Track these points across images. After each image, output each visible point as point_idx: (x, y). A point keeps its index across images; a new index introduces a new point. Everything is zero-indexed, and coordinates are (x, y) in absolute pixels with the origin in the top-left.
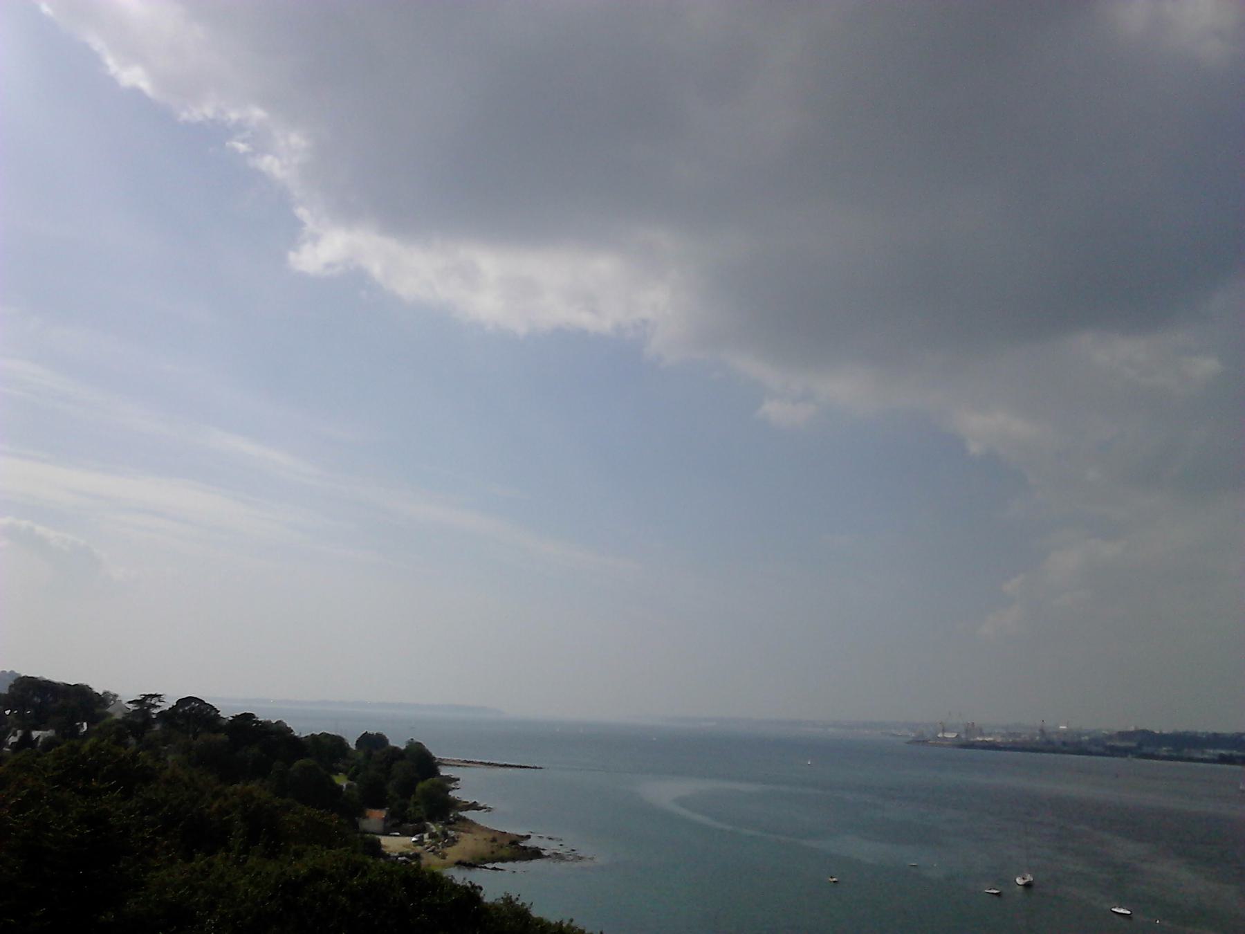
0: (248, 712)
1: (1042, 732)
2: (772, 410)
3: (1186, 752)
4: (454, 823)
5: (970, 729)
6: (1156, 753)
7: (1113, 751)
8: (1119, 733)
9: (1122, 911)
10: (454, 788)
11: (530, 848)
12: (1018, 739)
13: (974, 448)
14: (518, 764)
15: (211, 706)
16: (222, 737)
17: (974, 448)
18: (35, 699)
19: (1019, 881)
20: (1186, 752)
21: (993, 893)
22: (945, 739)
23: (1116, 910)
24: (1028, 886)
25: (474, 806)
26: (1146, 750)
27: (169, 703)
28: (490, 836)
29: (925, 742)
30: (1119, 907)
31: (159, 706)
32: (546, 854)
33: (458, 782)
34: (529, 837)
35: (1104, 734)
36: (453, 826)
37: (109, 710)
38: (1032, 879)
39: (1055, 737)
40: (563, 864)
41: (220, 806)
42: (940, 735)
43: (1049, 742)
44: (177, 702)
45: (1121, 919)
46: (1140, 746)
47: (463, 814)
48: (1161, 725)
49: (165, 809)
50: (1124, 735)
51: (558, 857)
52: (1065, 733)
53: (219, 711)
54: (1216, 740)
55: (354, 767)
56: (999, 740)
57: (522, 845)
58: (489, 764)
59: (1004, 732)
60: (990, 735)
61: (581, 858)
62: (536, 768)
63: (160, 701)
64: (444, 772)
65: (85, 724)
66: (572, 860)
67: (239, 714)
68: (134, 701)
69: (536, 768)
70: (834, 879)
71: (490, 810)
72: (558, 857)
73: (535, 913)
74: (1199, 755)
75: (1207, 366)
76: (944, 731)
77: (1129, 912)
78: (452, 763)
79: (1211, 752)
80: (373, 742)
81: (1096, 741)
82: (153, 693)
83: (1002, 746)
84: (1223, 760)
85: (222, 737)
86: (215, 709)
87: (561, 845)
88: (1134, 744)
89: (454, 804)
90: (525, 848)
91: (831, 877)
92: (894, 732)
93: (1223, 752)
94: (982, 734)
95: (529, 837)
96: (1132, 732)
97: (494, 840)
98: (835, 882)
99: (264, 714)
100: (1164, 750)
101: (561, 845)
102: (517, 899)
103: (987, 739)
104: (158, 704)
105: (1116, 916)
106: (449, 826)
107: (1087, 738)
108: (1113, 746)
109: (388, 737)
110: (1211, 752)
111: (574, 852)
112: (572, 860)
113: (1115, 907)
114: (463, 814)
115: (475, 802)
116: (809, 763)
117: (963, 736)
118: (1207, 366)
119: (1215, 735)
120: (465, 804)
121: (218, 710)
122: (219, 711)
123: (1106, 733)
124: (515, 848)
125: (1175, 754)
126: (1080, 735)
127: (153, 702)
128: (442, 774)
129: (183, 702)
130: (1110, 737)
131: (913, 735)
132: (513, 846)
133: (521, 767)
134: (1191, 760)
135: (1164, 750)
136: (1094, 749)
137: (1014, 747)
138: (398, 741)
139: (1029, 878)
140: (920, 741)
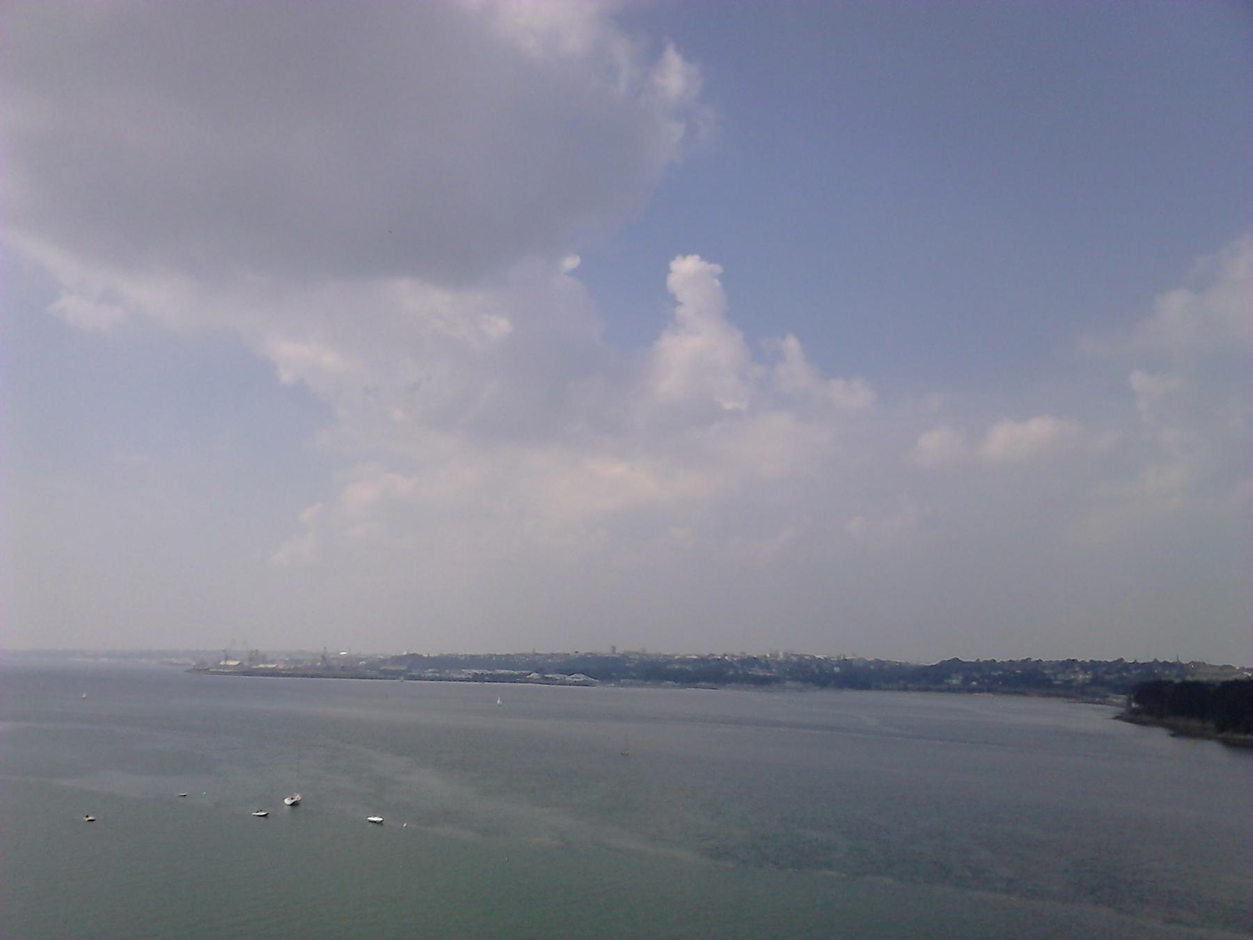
1: (324, 658)
5: (255, 656)
6: (422, 676)
7: (387, 675)
8: (393, 657)
12: (300, 666)
13: (286, 377)
17: (286, 377)
18: (835, 669)
19: (288, 801)
21: (375, 822)
22: (226, 667)
35: (380, 659)
42: (222, 663)
46: (409, 669)
48: (820, 651)
50: (398, 660)
52: (346, 658)
54: (473, 661)
56: (281, 667)
60: (273, 662)
70: (90, 818)
75: (500, 326)
76: (227, 659)
77: (381, 819)
84: (476, 678)
88: (404, 668)
94: (265, 662)
96: (405, 656)
100: (429, 672)
103: (270, 666)
105: (371, 825)
116: (84, 696)
117: (246, 664)
118: (500, 326)
119: (472, 656)
123: (382, 657)
126: (669, 662)
130: (384, 662)
135: (429, 672)
136: (369, 673)
139: (297, 797)
140: (201, 669)
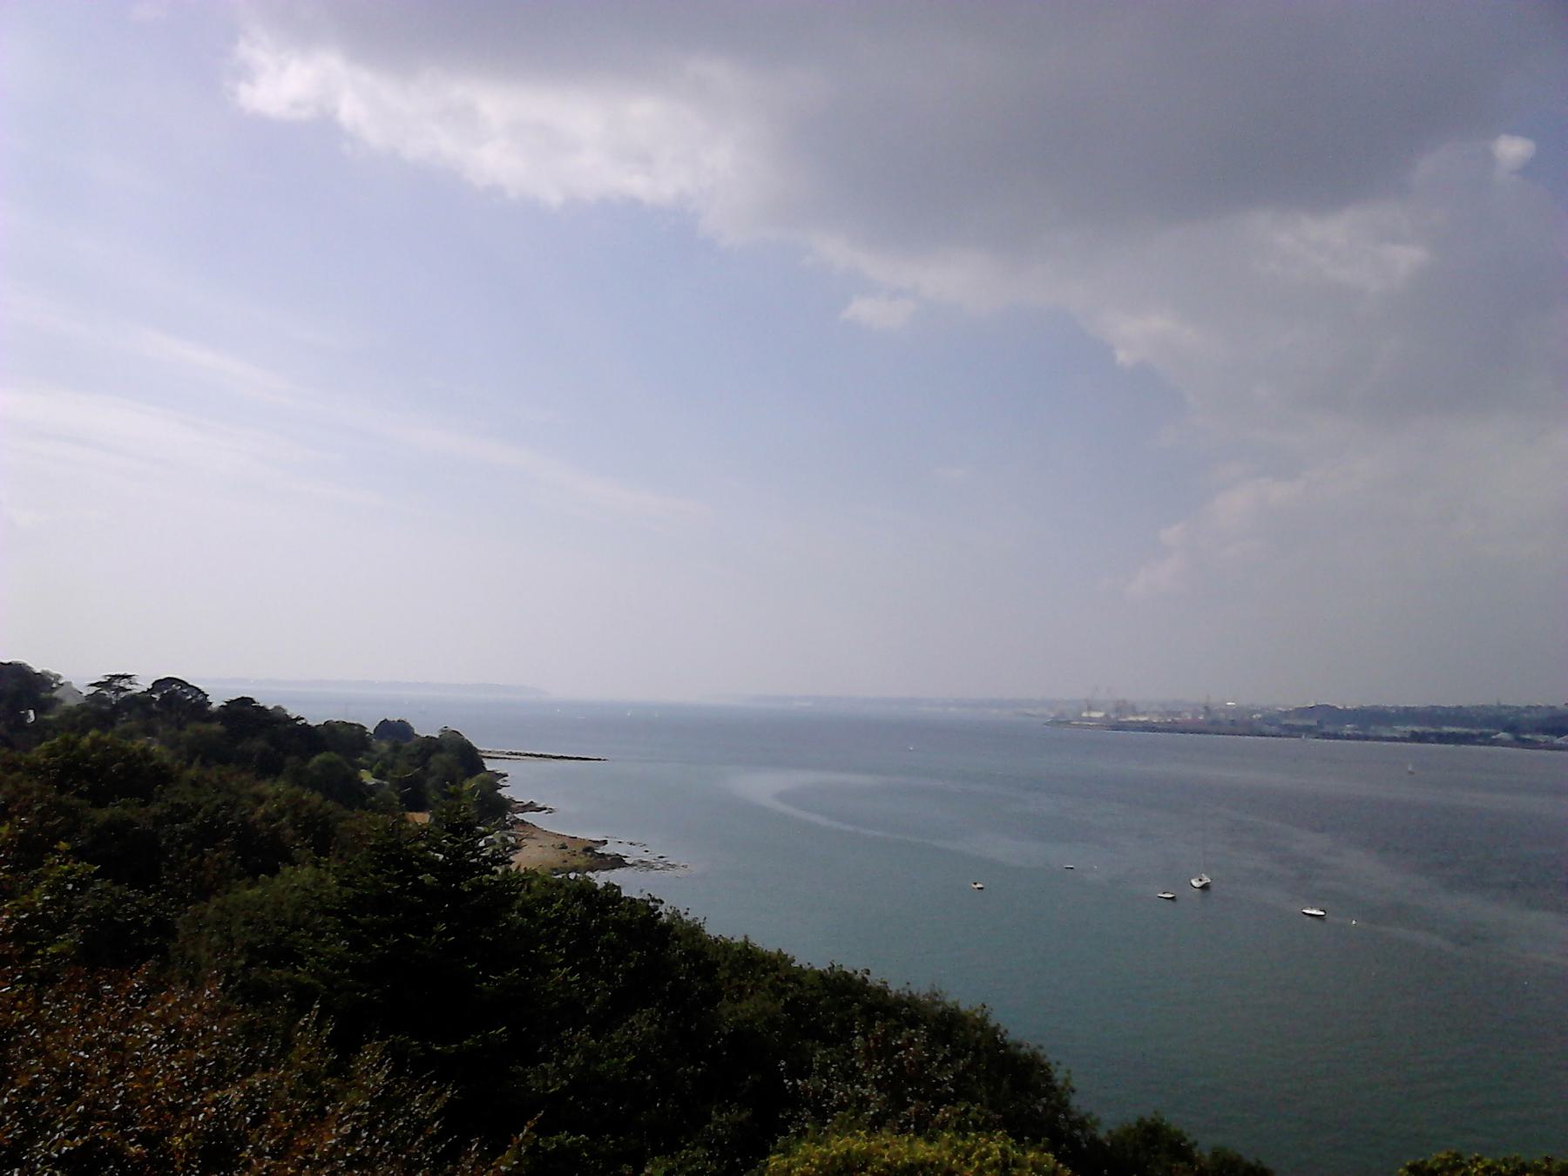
0: (246, 696)
2: (863, 309)
3: (1373, 730)
4: (511, 828)
5: (1121, 707)
7: (1292, 731)
9: (1314, 912)
10: (503, 786)
11: (609, 855)
14: (559, 755)
15: (197, 688)
16: (217, 727)
20: (1373, 730)
22: (1090, 719)
23: (1307, 911)
24: (1205, 887)
25: (531, 807)
26: (1329, 729)
27: (143, 684)
28: (559, 842)
29: (1068, 723)
30: (1312, 908)
31: (130, 690)
32: (630, 863)
33: (506, 778)
34: (605, 842)
36: (511, 831)
37: (56, 694)
38: (1209, 881)
39: (1222, 715)
40: (653, 872)
41: (266, 812)
42: (1085, 715)
43: (1215, 722)
44: (153, 684)
45: (1314, 920)
47: (520, 816)
49: (200, 815)
51: (648, 866)
53: (208, 695)
54: (1408, 715)
55: (379, 763)
57: (599, 852)
58: (541, 756)
59: (1161, 710)
60: (1144, 714)
61: (673, 866)
62: (600, 760)
63: (131, 683)
64: (490, 765)
65: (31, 713)
66: (662, 869)
67: (234, 698)
68: (98, 683)
69: (600, 760)
70: (979, 886)
71: (551, 811)
72: (648, 866)
73: (712, 930)
74: (1386, 733)
76: (1090, 709)
77: (1322, 913)
78: (496, 755)
79: (1401, 729)
80: (395, 730)
81: (1270, 719)
82: (122, 673)
83: (1160, 727)
85: (217, 727)
86: (203, 692)
87: (647, 851)
88: (1313, 723)
89: (505, 805)
90: (603, 855)
91: (975, 884)
92: (1029, 711)
93: (1416, 729)
94: (1136, 714)
95: (605, 842)
97: (564, 847)
98: (979, 888)
99: (266, 700)
100: (1348, 729)
101: (647, 851)
102: (686, 914)
103: (1142, 719)
104: (128, 687)
105: (1309, 918)
106: (507, 832)
107: (1259, 716)
108: (1293, 725)
109: (412, 724)
110: (1401, 729)
111: (664, 859)
112: (662, 869)
113: (1305, 908)
114: (520, 816)
115: (532, 802)
116: (911, 748)
118: (1408, 257)
119: (1407, 709)
120: (521, 804)
121: (206, 693)
122: (208, 695)
124: (591, 856)
125: (1360, 733)
127: (122, 684)
128: (488, 769)
129: (159, 684)
130: (1286, 714)
131: (1052, 715)
132: (589, 854)
133: (577, 758)
134: (1336, 736)
135: (1348, 729)
136: (1266, 728)
137: (1171, 728)
138: (425, 728)
139: (1206, 880)
